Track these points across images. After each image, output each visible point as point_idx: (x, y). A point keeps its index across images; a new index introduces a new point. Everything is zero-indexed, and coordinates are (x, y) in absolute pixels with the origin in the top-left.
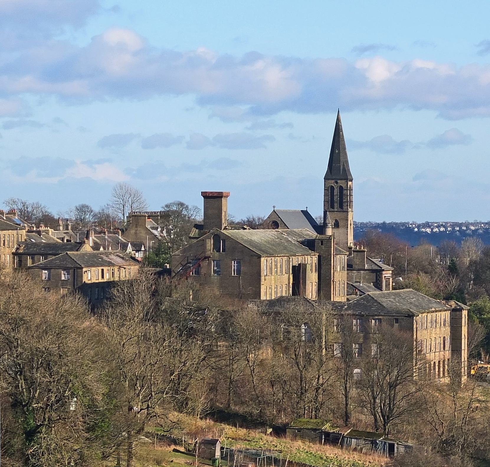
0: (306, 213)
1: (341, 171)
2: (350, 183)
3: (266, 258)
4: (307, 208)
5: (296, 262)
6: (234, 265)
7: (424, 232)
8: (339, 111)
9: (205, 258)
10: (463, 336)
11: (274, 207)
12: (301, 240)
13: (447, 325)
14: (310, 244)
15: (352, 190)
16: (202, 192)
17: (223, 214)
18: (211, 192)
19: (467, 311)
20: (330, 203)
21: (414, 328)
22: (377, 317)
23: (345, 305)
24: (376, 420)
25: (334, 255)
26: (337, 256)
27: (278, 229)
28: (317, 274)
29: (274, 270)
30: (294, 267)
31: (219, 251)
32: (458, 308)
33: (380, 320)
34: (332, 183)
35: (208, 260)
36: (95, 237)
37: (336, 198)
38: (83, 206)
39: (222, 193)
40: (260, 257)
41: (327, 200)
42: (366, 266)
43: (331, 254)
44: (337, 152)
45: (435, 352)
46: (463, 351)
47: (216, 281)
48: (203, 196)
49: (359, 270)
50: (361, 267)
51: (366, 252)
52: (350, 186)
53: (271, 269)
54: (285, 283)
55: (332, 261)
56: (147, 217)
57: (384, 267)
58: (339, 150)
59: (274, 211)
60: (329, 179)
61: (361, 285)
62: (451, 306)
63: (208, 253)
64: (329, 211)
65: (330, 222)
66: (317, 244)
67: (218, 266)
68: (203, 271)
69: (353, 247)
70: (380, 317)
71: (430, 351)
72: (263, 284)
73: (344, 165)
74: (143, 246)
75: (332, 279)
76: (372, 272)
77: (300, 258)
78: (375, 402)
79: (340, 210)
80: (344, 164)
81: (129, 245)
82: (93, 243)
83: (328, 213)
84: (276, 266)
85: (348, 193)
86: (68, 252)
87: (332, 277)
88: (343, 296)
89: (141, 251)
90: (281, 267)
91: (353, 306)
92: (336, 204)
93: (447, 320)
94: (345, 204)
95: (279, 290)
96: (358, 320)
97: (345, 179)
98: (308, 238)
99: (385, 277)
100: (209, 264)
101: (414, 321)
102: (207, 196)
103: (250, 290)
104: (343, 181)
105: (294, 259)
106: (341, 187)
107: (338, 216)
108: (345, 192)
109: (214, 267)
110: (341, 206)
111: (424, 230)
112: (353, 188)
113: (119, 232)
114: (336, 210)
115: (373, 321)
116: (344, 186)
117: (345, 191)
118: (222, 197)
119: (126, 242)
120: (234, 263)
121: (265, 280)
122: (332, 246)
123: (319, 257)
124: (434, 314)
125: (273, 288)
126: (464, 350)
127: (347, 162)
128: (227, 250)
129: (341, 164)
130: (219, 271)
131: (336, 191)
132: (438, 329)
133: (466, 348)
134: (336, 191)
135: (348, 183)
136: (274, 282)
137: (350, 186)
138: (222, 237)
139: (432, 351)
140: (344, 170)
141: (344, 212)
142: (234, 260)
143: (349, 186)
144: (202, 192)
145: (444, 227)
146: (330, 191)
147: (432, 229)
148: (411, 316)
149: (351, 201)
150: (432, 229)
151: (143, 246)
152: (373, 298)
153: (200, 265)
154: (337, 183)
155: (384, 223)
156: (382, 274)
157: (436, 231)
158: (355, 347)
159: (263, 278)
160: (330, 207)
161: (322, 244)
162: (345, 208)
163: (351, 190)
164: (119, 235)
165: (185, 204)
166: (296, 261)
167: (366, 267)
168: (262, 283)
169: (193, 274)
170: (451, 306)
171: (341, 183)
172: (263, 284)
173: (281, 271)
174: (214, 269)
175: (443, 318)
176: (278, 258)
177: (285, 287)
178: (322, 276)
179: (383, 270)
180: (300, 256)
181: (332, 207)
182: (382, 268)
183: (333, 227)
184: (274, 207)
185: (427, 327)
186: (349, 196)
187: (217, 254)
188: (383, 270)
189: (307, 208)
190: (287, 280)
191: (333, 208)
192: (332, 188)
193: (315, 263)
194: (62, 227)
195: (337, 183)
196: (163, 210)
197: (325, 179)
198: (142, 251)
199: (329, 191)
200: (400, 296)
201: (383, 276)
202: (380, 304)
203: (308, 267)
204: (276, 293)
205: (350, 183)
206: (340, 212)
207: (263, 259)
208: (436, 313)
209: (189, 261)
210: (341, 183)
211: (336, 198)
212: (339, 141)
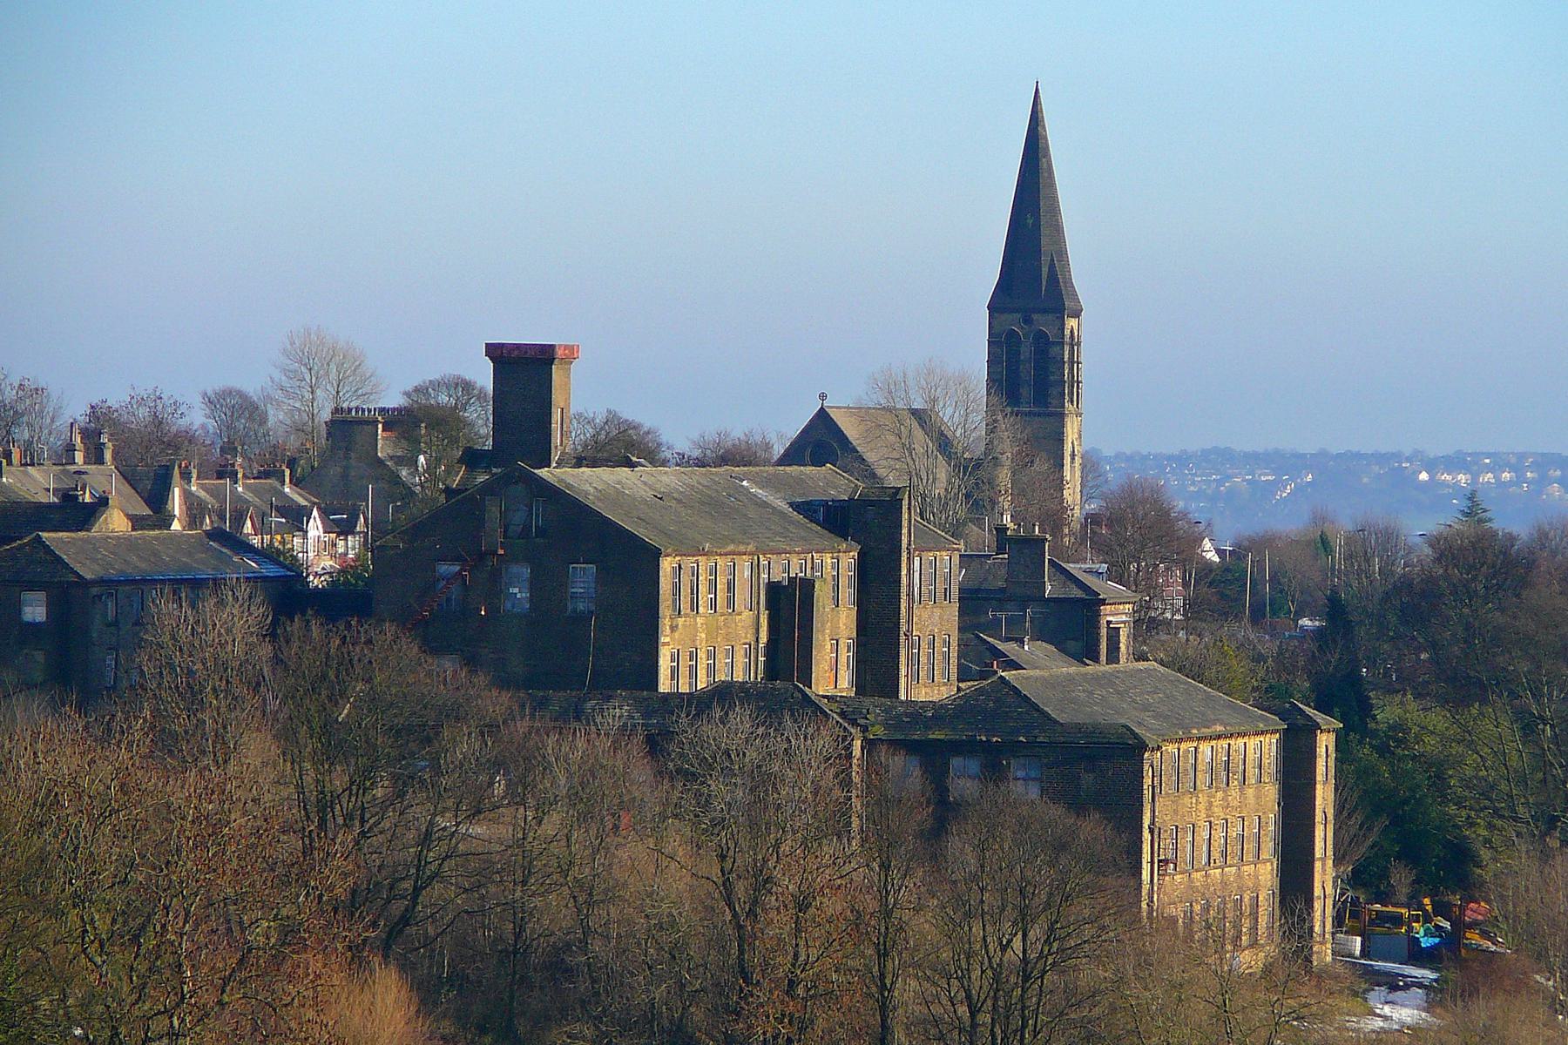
1: (1044, 283)
3: (678, 558)
5: (946, 568)
7: (1448, 486)
8: (1037, 90)
10: (1319, 817)
11: (823, 397)
13: (1265, 779)
15: (1079, 344)
17: (556, 416)
19: (1332, 736)
21: (1145, 787)
26: (924, 554)
27: (549, 467)
29: (704, 596)
30: (773, 588)
36: (203, 487)
37: (1027, 371)
40: (655, 555)
41: (999, 377)
42: (1048, 588)
46: (1318, 865)
52: (1072, 332)
54: (742, 641)
55: (904, 572)
56: (380, 426)
57: (1108, 588)
58: (1038, 219)
69: (1011, 526)
72: (667, 644)
73: (1052, 266)
74: (361, 516)
75: (904, 628)
77: (795, 561)
80: (1052, 260)
81: (315, 513)
82: (184, 508)
85: (1066, 353)
86: (44, 535)
87: (903, 621)
88: (945, 684)
89: (353, 533)
90: (731, 587)
93: (1265, 761)
95: (722, 661)
98: (13, 498)
99: (1109, 623)
101: (1146, 767)
104: (1050, 317)
105: (777, 562)
106: (1041, 336)
108: (1054, 350)
111: (1449, 478)
112: (1082, 339)
113: (284, 471)
119: (306, 503)
121: (673, 628)
122: (905, 523)
124: (1224, 743)
125: (702, 655)
126: (1323, 860)
127: (1062, 253)
129: (1045, 259)
131: (1026, 351)
132: (1234, 792)
133: (1330, 853)
134: (1026, 351)
136: (704, 636)
137: (1072, 332)
139: (1212, 861)
140: (1053, 279)
141: (1051, 415)
143: (1067, 332)
145: (1512, 468)
151: (361, 516)
154: (1028, 321)
155: (1323, 454)
156: (1098, 614)
157: (1488, 482)
163: (1075, 343)
164: (283, 483)
168: (663, 639)
172: (667, 644)
173: (731, 602)
175: (1252, 755)
176: (721, 561)
177: (743, 652)
179: (1103, 602)
184: (823, 397)
185: (1198, 783)
186: (1066, 365)
188: (1103, 602)
190: (751, 631)
194: (82, 454)
195: (1028, 321)
198: (360, 533)
199: (1002, 346)
200: (1112, 684)
201: (1103, 622)
203: (822, 593)
204: (711, 670)
205: (1071, 323)
207: (667, 565)
208: (1228, 741)
210: (1043, 323)
211: (1027, 371)
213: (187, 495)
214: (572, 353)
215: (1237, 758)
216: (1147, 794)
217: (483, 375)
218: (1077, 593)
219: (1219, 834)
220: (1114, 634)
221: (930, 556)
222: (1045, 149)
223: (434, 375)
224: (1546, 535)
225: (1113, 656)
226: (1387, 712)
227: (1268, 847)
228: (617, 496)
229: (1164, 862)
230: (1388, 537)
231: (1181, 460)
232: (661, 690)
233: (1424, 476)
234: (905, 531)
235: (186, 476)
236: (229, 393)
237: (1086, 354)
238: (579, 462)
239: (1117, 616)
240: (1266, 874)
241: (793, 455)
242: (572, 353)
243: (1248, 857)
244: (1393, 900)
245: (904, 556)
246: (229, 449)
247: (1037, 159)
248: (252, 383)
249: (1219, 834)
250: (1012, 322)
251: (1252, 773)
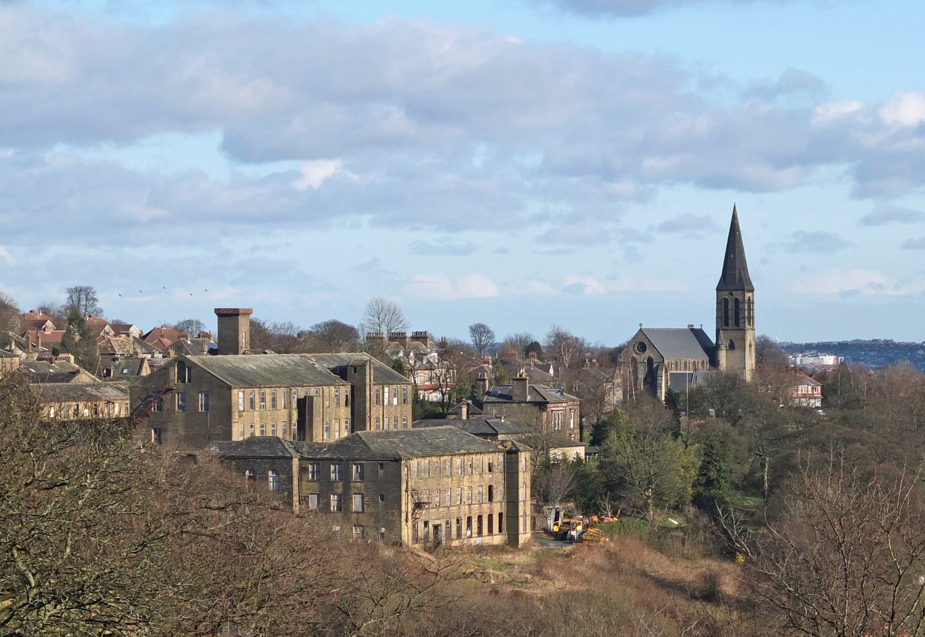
0: (699, 334)
1: (737, 279)
2: (748, 295)
4: (701, 325)
6: (201, 398)
11: (641, 325)
12: (333, 366)
15: (753, 303)
16: (215, 309)
18: (226, 309)
20: (723, 319)
22: (358, 462)
23: (325, 448)
25: (370, 385)
28: (350, 409)
31: (184, 381)
32: (514, 449)
33: (362, 465)
34: (725, 294)
35: (172, 393)
37: (731, 314)
38: (481, 326)
39: (237, 309)
40: (230, 388)
43: (365, 385)
44: (732, 256)
45: (470, 505)
47: (180, 418)
48: (217, 314)
49: (520, 403)
50: (522, 399)
51: (527, 381)
58: (735, 255)
59: (640, 329)
60: (722, 290)
61: (503, 421)
62: (506, 447)
63: (172, 385)
64: (723, 330)
66: (350, 371)
67: (183, 400)
68: (166, 406)
70: (362, 462)
71: (461, 503)
73: (740, 273)
76: (534, 405)
79: (735, 327)
83: (721, 331)
87: (368, 412)
91: (334, 449)
92: (730, 321)
94: (741, 321)
96: (337, 466)
97: (740, 290)
100: (173, 397)
102: (221, 313)
103: (219, 429)
104: (739, 292)
105: (301, 390)
106: (737, 300)
107: (734, 335)
108: (741, 306)
109: (178, 401)
110: (737, 323)
114: (731, 328)
115: (354, 467)
116: (740, 298)
117: (742, 304)
118: (237, 315)
120: (202, 396)
123: (352, 387)
126: (524, 501)
128: (192, 380)
129: (737, 271)
130: (185, 407)
131: (731, 305)
134: (731, 305)
135: (744, 295)
136: (258, 419)
138: (187, 364)
139: (462, 503)
140: (741, 279)
141: (740, 330)
142: (202, 392)
144: (215, 309)
146: (723, 305)
148: (397, 460)
152: (360, 438)
153: (162, 400)
154: (731, 294)
158: (334, 499)
159: (235, 416)
160: (723, 324)
161: (355, 372)
162: (741, 325)
165: (193, 321)
167: (529, 398)
169: (154, 409)
170: (506, 447)
174: (178, 404)
178: (356, 411)
180: (313, 386)
181: (727, 324)
182: (546, 400)
183: (728, 348)
184: (641, 325)
187: (181, 385)
188: (548, 403)
189: (701, 325)
191: (728, 326)
192: (726, 301)
193: (347, 395)
195: (731, 294)
196: (310, 329)
197: (719, 289)
199: (722, 305)
202: (366, 445)
205: (748, 295)
206: (736, 330)
209: (150, 394)
211: (731, 314)
232: (234, 439)
234: (368, 377)
236: (117, 321)
237: (757, 307)
245: (368, 387)
247: (735, 233)
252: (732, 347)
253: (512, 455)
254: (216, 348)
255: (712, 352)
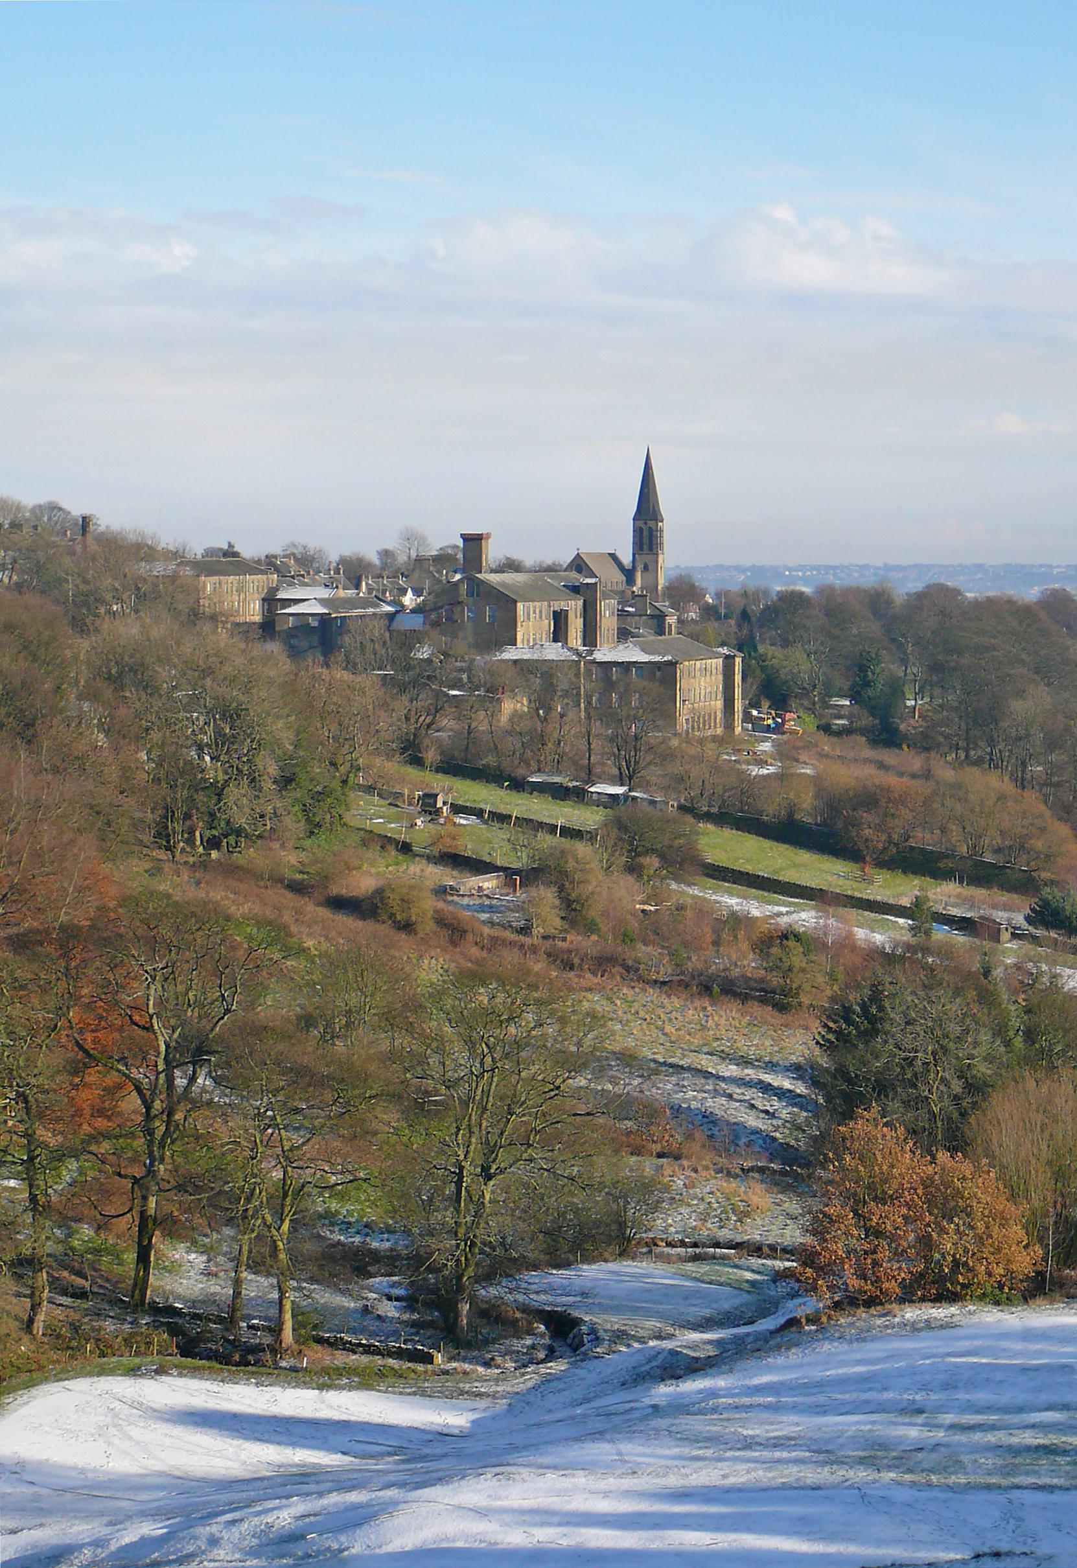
0: (613, 556)
2: (660, 524)
9: (459, 603)
14: (576, 590)
24: (621, 773)
31: (473, 596)
34: (640, 523)
37: (646, 540)
40: (515, 602)
50: (643, 613)
53: (529, 614)
65: (640, 567)
73: (654, 508)
78: (619, 754)
84: (535, 612)
90: (541, 612)
107: (648, 558)
108: (655, 533)
110: (651, 549)
127: (657, 501)
131: (645, 533)
132: (708, 678)
134: (645, 533)
145: (817, 570)
147: (804, 573)
149: (662, 544)
150: (804, 573)
154: (646, 523)
159: (519, 624)
163: (662, 531)
166: (558, 605)
167: (649, 612)
171: (651, 524)
181: (641, 549)
195: (646, 523)
199: (638, 533)
203: (571, 615)
205: (660, 524)
207: (520, 605)
210: (651, 524)
211: (646, 540)
212: (648, 480)
213: (367, 584)
214: (488, 536)
215: (709, 667)
216: (678, 679)
217: (460, 543)
218: (658, 612)
219: (703, 692)
220: (670, 626)
221: (607, 601)
222: (942, 588)
223: (446, 544)
224: (452, 758)
225: (670, 634)
226: (761, 649)
227: (720, 695)
228: (504, 584)
229: (684, 701)
230: (766, 592)
231: (701, 570)
233: (787, 573)
235: (367, 578)
238: (493, 571)
239: (672, 620)
240: (719, 704)
241: (569, 568)
242: (488, 536)
243: (713, 698)
244: (374, 1194)
246: (383, 569)
248: (390, 546)
249: (703, 692)
250: (640, 523)
251: (714, 671)
252: (646, 568)
253: (729, 659)
254: (88, 549)
255: (629, 575)
